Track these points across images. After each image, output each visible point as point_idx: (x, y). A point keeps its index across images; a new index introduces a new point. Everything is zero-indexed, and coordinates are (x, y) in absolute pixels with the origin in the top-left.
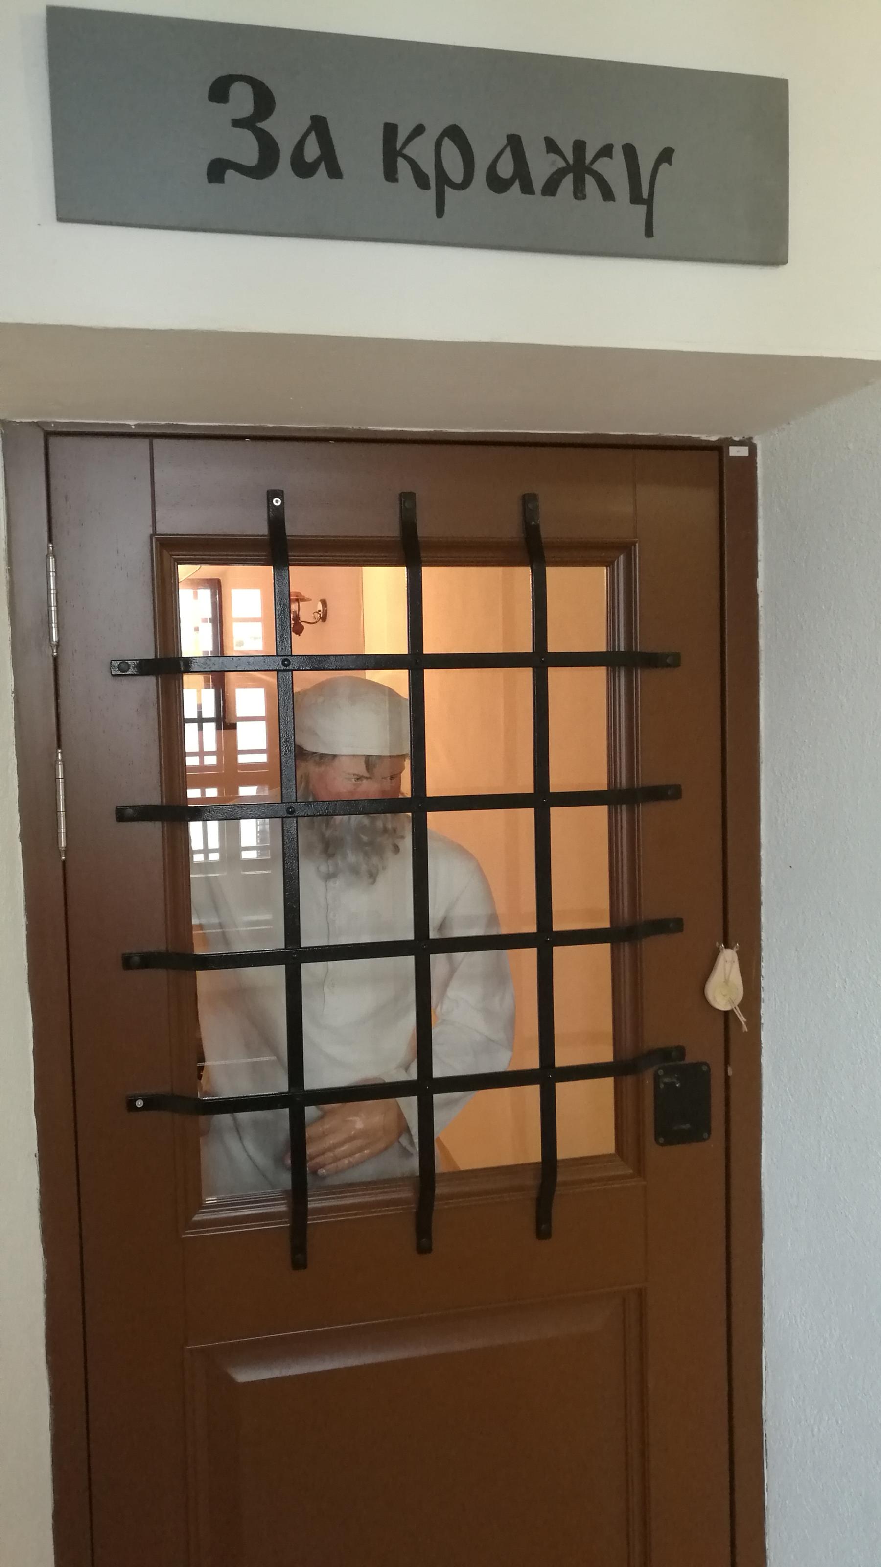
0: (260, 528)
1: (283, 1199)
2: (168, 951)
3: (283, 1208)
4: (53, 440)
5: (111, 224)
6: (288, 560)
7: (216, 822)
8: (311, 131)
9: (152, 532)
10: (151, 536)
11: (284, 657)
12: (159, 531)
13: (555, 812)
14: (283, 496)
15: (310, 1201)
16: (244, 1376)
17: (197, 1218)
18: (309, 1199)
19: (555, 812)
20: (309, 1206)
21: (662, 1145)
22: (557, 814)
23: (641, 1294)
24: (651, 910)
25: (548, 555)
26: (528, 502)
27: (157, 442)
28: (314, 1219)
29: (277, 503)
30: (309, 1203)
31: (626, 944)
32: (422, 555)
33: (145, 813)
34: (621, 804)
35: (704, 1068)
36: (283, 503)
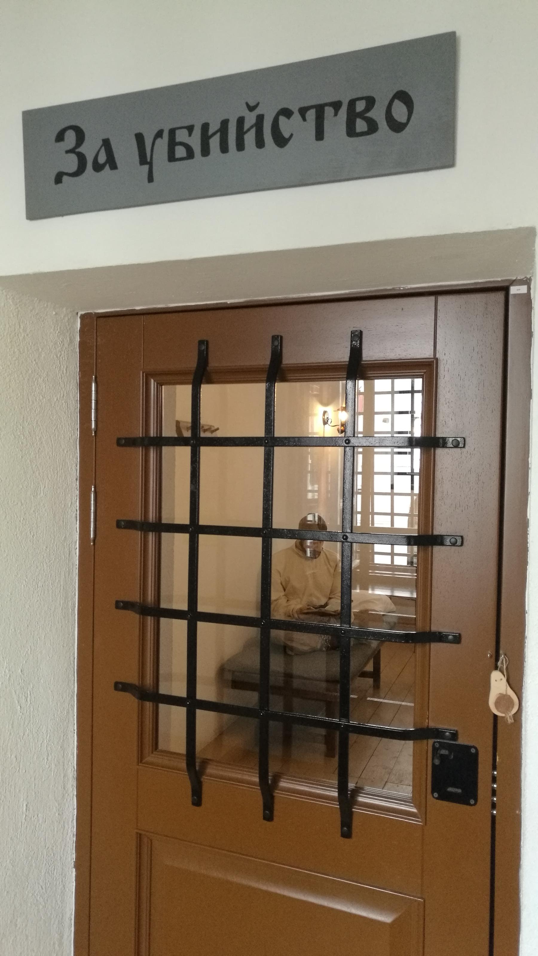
27: (442, 299)
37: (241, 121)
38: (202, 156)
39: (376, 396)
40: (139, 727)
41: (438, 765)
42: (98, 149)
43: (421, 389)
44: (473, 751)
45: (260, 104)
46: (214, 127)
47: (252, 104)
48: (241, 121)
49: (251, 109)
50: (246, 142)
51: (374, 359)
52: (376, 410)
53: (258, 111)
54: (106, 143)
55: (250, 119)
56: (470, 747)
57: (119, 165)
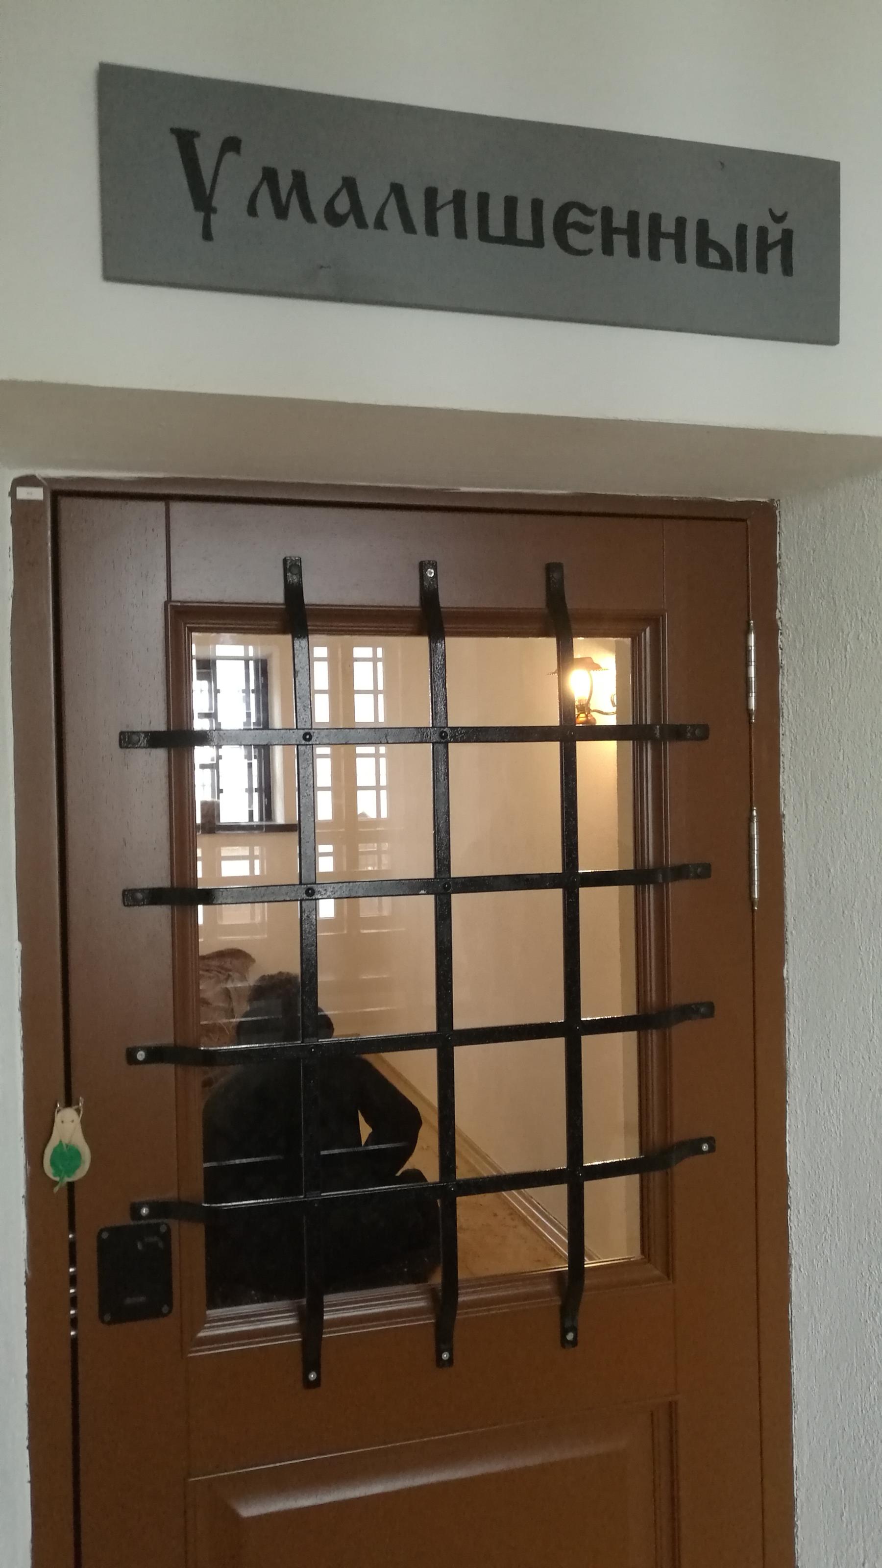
0: (411, 599)
1: (421, 1294)
2: (175, 1044)
3: (291, 1322)
4: (65, 503)
5: (605, 323)
6: (307, 630)
7: (332, 901)
8: (779, 244)
9: (166, 599)
10: (166, 604)
11: (307, 731)
12: (177, 596)
13: (558, 893)
14: (436, 565)
15: (327, 1312)
16: (249, 1510)
17: (201, 1334)
18: (325, 1309)
19: (558, 893)
20: (325, 1318)
21: (109, 1323)
22: (457, 900)
23: (672, 1409)
24: (678, 997)
25: (447, 626)
26: (292, 567)
27: (177, 508)
28: (330, 1332)
29: (432, 573)
30: (325, 1314)
31: (654, 1031)
32: (446, 626)
33: (155, 896)
34: (649, 884)
35: (105, 1235)
36: (436, 574)
37: (762, 232)
38: (203, 237)
39: (355, 663)
40: (679, 1557)
41: (441, 1356)
42: (334, 190)
43: (370, 649)
44: (165, 1309)
45: (789, 215)
46: (620, 220)
47: (779, 213)
48: (762, 232)
49: (778, 219)
50: (770, 264)
51: (265, 601)
52: (356, 688)
53: (785, 225)
54: (350, 184)
55: (775, 233)
56: (171, 1306)
57: (440, 230)
